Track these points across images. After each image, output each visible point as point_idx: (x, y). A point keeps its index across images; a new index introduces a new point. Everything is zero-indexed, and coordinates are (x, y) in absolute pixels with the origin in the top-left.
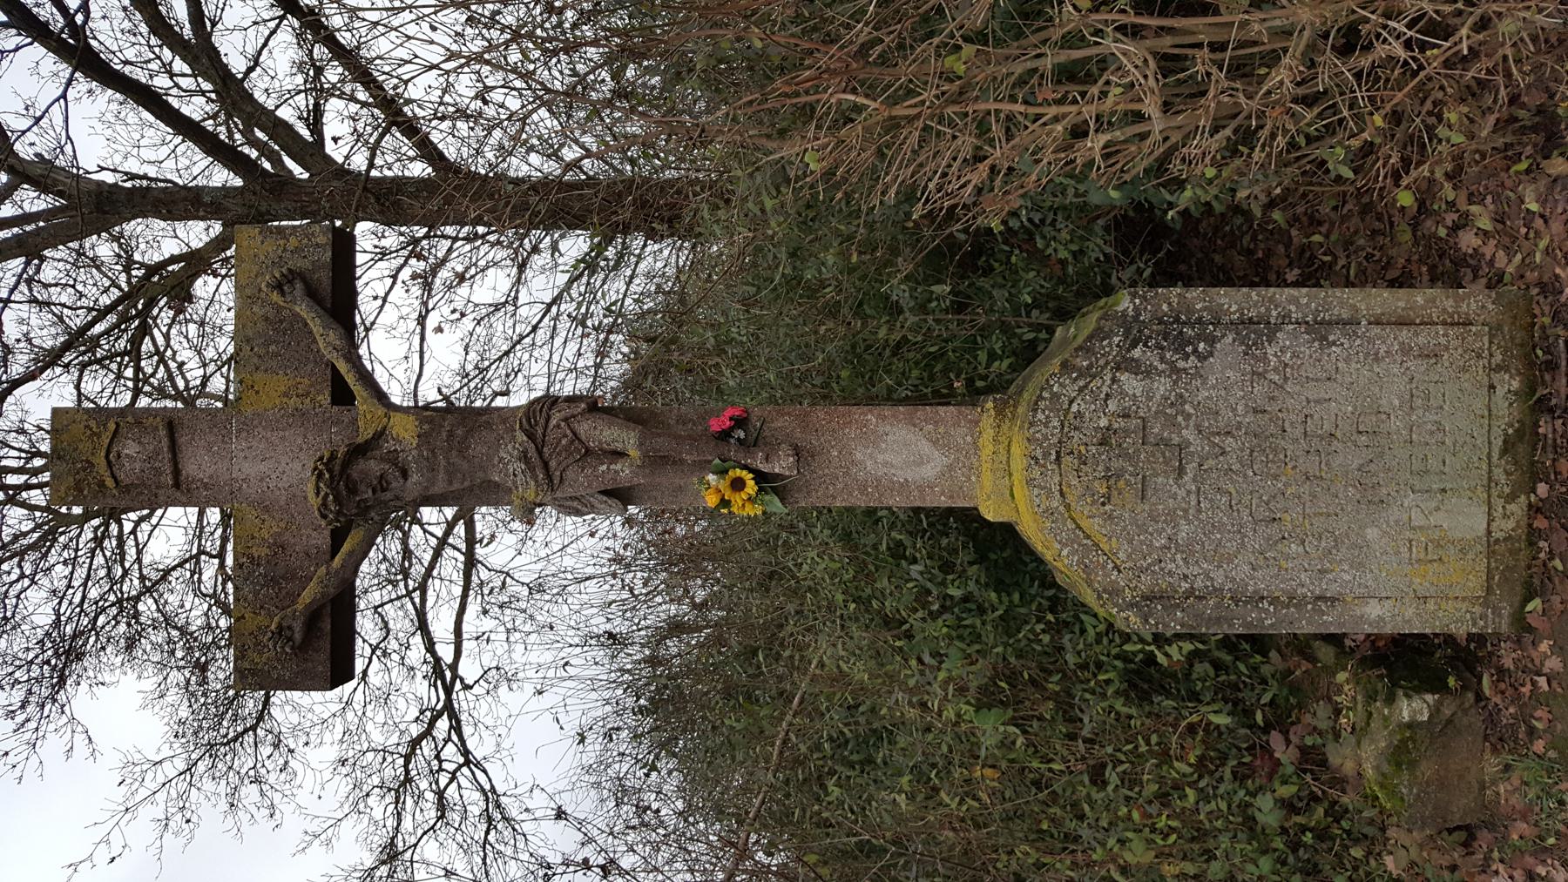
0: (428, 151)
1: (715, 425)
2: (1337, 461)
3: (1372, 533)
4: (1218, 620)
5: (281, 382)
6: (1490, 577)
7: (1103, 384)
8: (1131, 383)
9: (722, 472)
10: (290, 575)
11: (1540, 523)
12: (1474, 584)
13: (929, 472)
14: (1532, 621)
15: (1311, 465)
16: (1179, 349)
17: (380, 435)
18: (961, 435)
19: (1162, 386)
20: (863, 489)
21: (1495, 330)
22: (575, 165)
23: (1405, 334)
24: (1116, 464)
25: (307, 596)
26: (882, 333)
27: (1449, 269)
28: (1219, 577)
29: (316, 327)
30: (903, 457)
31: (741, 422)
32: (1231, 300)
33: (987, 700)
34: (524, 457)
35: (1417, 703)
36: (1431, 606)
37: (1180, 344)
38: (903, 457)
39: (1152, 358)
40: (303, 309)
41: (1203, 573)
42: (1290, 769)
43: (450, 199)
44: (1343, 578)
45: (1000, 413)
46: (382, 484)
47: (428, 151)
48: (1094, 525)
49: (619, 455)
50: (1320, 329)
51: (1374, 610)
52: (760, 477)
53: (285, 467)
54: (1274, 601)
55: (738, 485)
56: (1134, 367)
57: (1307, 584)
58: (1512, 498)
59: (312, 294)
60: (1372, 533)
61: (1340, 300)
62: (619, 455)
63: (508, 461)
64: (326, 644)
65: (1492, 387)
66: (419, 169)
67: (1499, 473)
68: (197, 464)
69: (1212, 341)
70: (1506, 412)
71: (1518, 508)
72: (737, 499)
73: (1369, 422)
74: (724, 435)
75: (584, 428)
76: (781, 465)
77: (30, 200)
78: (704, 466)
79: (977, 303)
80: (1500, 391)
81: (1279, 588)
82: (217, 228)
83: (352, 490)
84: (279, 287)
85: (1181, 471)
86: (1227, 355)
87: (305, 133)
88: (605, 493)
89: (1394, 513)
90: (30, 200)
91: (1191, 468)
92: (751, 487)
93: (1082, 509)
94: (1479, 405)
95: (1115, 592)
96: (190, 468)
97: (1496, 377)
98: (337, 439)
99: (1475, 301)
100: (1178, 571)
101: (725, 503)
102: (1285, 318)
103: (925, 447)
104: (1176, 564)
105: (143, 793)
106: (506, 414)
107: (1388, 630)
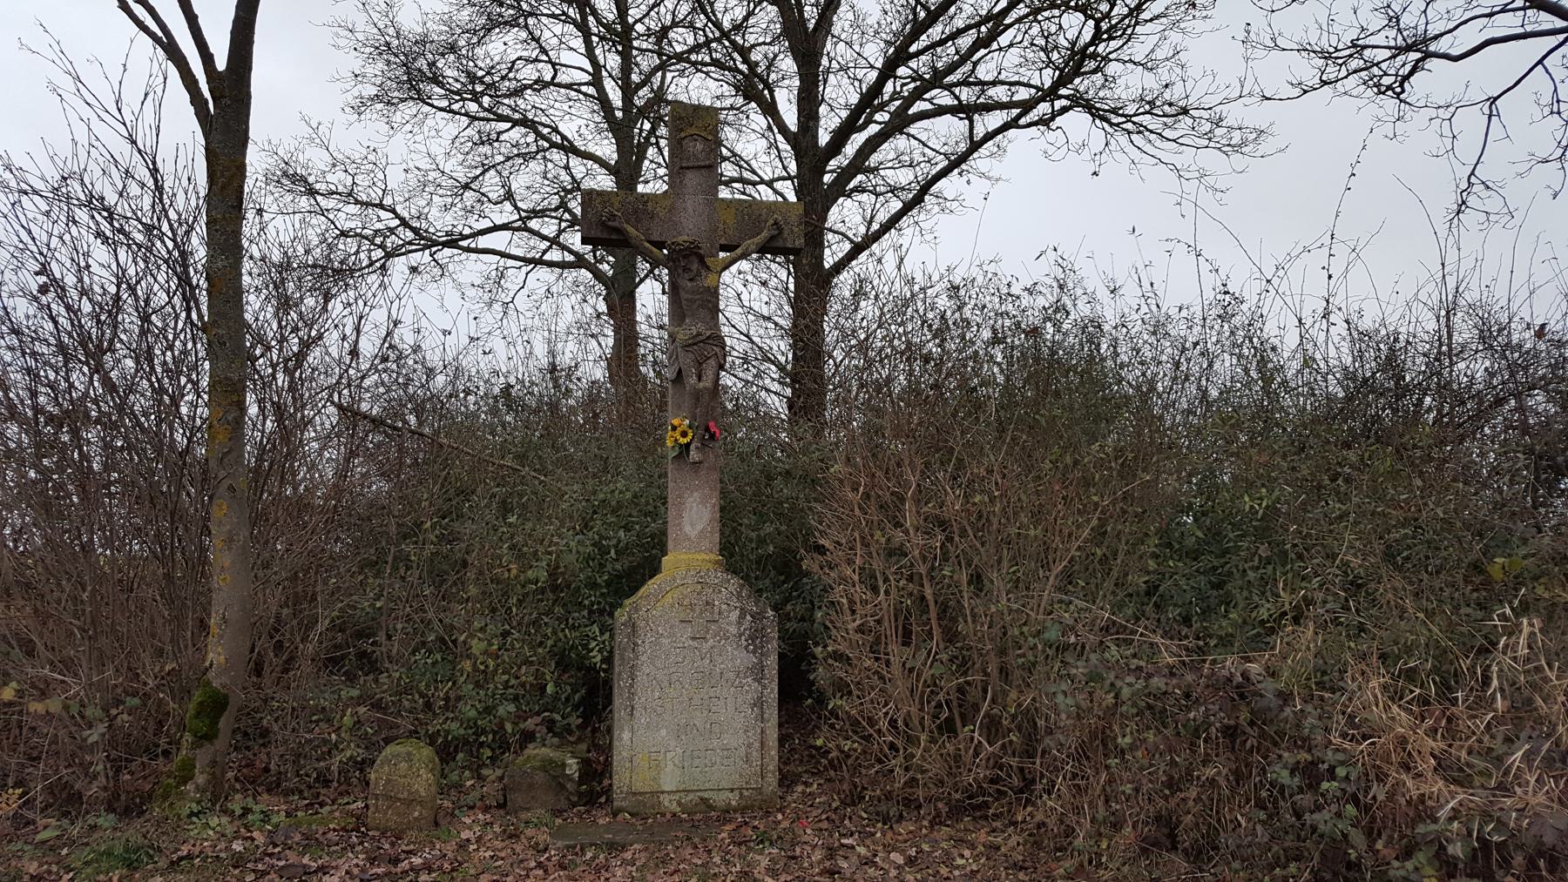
0: (839, 267)
1: (711, 424)
2: (698, 713)
3: (664, 732)
4: (622, 659)
5: (731, 221)
6: (641, 794)
7: (734, 602)
8: (735, 615)
9: (690, 427)
10: (638, 220)
11: (668, 816)
12: (638, 786)
13: (687, 529)
14: (620, 817)
15: (696, 701)
16: (750, 637)
17: (708, 268)
18: (706, 544)
19: (733, 630)
20: (679, 496)
21: (759, 790)
22: (831, 357)
23: (757, 745)
24: (697, 609)
25: (630, 229)
26: (746, 521)
27: (787, 780)
28: (643, 658)
29: (756, 240)
30: (694, 519)
31: (712, 437)
32: (772, 662)
33: (553, 573)
34: (699, 334)
35: (575, 767)
36: (628, 765)
37: (752, 638)
38: (694, 519)
39: (746, 625)
40: (765, 234)
41: (646, 652)
42: (522, 726)
43: (812, 287)
44: (642, 719)
45: (717, 562)
46: (686, 269)
47: (839, 267)
48: (669, 599)
49: (700, 379)
50: (759, 703)
51: (626, 736)
52: (688, 445)
53: (690, 225)
54: (632, 686)
55: (684, 434)
56: (742, 616)
57: (638, 702)
58: (679, 804)
59: (772, 238)
60: (664, 732)
61: (772, 715)
62: (700, 379)
63: (695, 327)
64: (605, 236)
65: (732, 790)
66: (828, 262)
67: (691, 796)
68: (692, 179)
69: (754, 652)
70: (720, 799)
71: (675, 807)
72: (677, 434)
73: (716, 729)
74: (707, 429)
75: (712, 362)
76: (694, 455)
77: (811, 13)
78: (693, 418)
79: (770, 560)
80: (730, 795)
81: (638, 687)
82: (793, 128)
83: (684, 257)
84: (776, 223)
85: (694, 639)
86: (744, 659)
87: (851, 185)
88: (680, 371)
89: (673, 743)
90: (811, 13)
91: (695, 644)
92: (683, 441)
93: (676, 594)
94: (724, 784)
95: (637, 610)
96: (690, 175)
97: (737, 792)
98: (705, 248)
99: (772, 780)
100: (646, 640)
101: (674, 428)
102: (764, 687)
103: (699, 527)
104: (650, 638)
105: (375, 16)
106: (717, 325)
107: (616, 743)
